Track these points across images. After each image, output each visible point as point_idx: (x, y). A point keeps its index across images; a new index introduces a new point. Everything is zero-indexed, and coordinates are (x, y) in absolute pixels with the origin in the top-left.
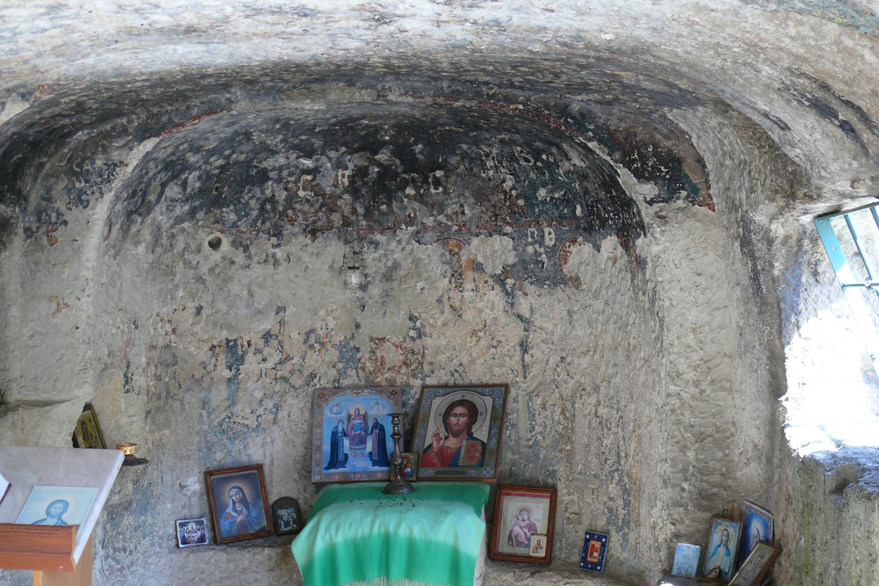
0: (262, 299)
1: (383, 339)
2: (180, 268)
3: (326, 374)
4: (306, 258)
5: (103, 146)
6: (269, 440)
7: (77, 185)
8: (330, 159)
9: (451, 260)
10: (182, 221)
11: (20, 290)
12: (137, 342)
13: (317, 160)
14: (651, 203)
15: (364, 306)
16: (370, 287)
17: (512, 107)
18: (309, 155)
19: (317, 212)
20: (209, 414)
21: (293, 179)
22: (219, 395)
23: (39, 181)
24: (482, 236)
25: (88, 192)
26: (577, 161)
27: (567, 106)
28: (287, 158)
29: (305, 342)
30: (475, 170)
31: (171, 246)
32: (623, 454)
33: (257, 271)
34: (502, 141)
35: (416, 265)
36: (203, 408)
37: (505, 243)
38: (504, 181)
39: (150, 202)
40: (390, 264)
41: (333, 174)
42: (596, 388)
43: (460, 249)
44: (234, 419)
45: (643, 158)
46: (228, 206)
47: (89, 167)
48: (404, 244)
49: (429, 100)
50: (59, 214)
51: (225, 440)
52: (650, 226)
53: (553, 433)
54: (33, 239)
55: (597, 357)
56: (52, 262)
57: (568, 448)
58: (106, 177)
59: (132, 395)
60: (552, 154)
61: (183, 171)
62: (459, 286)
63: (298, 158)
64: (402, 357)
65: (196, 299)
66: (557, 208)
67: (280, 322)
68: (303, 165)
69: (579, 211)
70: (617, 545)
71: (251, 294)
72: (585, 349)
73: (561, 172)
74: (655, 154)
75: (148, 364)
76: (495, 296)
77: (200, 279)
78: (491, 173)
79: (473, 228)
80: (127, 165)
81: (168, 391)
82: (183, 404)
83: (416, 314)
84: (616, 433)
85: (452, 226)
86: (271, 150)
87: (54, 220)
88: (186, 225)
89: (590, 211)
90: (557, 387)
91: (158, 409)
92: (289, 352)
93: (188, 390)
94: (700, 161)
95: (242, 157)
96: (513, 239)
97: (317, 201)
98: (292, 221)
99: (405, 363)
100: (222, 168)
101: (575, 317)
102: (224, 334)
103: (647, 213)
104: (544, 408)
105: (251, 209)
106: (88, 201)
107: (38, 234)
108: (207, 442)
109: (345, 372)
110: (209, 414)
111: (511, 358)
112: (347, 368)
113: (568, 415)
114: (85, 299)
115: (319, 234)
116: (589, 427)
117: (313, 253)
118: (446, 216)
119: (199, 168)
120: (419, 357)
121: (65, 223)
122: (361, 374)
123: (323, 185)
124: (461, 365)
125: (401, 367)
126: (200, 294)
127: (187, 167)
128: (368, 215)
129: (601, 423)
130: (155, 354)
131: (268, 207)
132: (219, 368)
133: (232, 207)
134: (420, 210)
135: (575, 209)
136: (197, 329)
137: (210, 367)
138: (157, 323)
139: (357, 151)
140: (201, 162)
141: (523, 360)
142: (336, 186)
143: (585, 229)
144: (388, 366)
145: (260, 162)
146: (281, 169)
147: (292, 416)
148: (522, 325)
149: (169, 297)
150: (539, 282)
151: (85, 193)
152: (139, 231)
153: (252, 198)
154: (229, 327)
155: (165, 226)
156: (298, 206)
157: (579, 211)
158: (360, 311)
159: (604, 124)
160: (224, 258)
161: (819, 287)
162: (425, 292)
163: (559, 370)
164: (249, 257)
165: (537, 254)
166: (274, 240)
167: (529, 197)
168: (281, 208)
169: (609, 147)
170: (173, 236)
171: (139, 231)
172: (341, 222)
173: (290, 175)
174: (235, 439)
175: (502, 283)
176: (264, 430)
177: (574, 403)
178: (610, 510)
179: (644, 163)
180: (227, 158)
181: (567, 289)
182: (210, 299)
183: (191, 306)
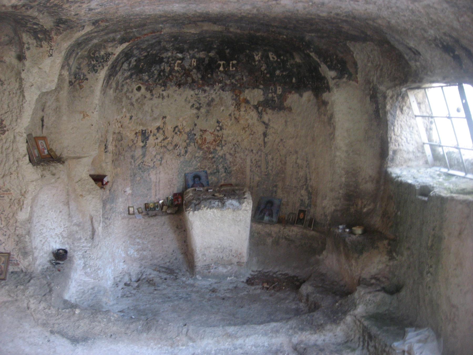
1: (206, 131)
2: (124, 99)
3: (182, 144)
4: (175, 96)
5: (104, 46)
6: (158, 172)
7: (92, 62)
8: (190, 54)
9: (236, 98)
10: (127, 79)
11: (67, 109)
13: (185, 54)
14: (333, 79)
15: (198, 117)
16: (201, 109)
18: (181, 52)
19: (182, 76)
20: (134, 161)
21: (173, 62)
22: (138, 152)
24: (250, 89)
25: (97, 66)
26: (298, 60)
29: (174, 131)
30: (250, 61)
31: (122, 89)
32: (308, 179)
33: (156, 101)
36: (132, 159)
38: (262, 66)
39: (117, 71)
40: (210, 99)
41: (190, 61)
42: (296, 152)
44: (144, 163)
46: (145, 73)
47: (98, 55)
50: (84, 75)
51: (141, 172)
54: (73, 86)
56: (81, 97)
58: (105, 59)
59: (108, 154)
61: (130, 58)
62: (239, 109)
64: (213, 138)
65: (130, 113)
67: (164, 123)
68: (178, 56)
69: (294, 80)
75: (113, 140)
76: (254, 114)
77: (132, 104)
79: (246, 86)
80: (114, 54)
81: (119, 152)
82: (124, 158)
83: (220, 120)
85: (237, 84)
87: (82, 78)
88: (128, 81)
90: (278, 151)
93: (126, 151)
94: (355, 64)
95: (154, 52)
96: (263, 91)
98: (171, 80)
100: (146, 57)
101: (288, 123)
102: (141, 128)
103: (331, 83)
105: (155, 75)
106: (97, 70)
107: (75, 84)
109: (189, 144)
110: (134, 161)
111: (259, 139)
112: (190, 142)
113: (283, 162)
114: (95, 113)
115: (182, 86)
116: (293, 167)
117: (178, 94)
119: (137, 56)
120: (220, 138)
121: (87, 79)
122: (196, 144)
123: (185, 65)
124: (238, 141)
125: (213, 142)
126: (131, 110)
127: (132, 56)
128: (203, 78)
129: (298, 166)
130: (115, 136)
131: (162, 74)
132: (138, 142)
133: (147, 73)
135: (292, 79)
136: (130, 125)
137: (135, 142)
139: (202, 51)
140: (138, 54)
141: (264, 140)
142: (190, 65)
144: (207, 141)
145: (161, 55)
146: (169, 58)
147: (168, 162)
148: (264, 126)
149: (120, 112)
150: (273, 108)
151: (96, 66)
153: (155, 70)
154: (142, 124)
155: (120, 81)
156: (174, 74)
157: (294, 80)
158: (196, 119)
160: (142, 95)
161: (403, 116)
162: (224, 112)
164: (152, 95)
165: (273, 97)
166: (163, 88)
167: (272, 74)
168: (167, 74)
170: (123, 86)
171: (112, 83)
172: (191, 81)
173: (172, 60)
174: (145, 171)
176: (156, 168)
177: (286, 158)
178: (302, 200)
183: (128, 115)
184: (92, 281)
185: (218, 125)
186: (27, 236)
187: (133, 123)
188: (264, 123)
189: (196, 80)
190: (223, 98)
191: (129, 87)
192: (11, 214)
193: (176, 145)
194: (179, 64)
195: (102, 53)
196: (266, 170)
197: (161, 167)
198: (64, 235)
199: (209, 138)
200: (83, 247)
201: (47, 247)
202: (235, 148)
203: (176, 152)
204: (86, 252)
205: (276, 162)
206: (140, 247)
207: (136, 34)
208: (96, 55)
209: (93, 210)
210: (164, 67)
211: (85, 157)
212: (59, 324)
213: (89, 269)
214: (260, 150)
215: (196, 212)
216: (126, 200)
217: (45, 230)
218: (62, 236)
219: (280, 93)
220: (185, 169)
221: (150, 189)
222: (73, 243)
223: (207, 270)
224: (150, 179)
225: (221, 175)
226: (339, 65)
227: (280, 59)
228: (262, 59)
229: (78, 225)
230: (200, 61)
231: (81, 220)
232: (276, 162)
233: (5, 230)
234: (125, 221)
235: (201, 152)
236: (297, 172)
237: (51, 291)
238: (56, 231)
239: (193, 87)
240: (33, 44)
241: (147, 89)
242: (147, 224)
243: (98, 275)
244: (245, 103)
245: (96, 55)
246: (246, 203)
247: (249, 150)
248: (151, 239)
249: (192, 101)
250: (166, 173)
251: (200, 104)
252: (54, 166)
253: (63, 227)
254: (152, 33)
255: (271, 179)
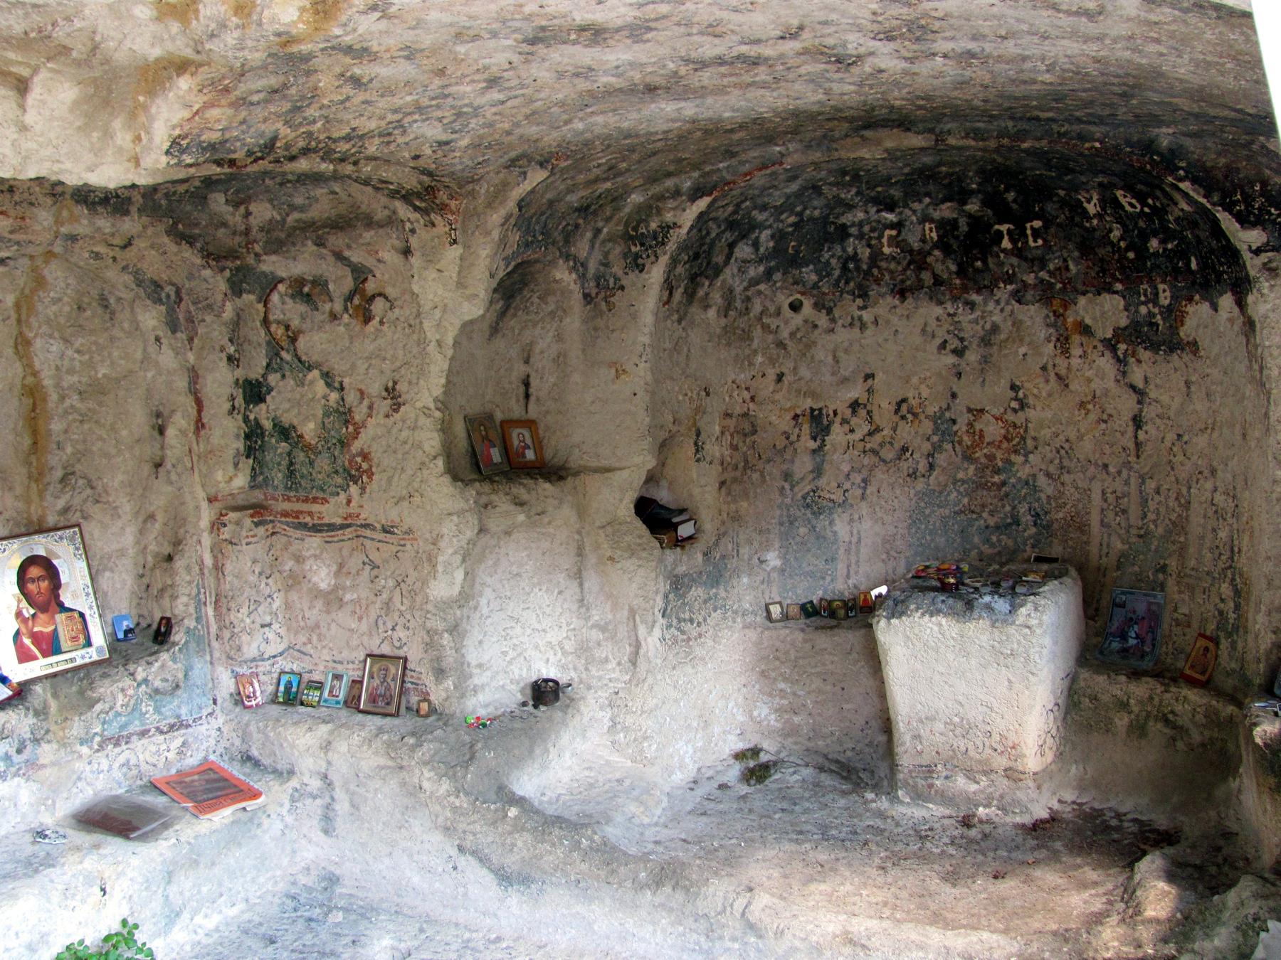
0: (846, 370)
1: (982, 411)
2: (757, 332)
3: (920, 447)
4: (895, 320)
5: (657, 207)
6: (856, 517)
8: (914, 212)
9: (1056, 322)
10: (758, 283)
12: (709, 410)
13: (901, 213)
14: (1257, 252)
17: (1087, 145)
18: (891, 209)
20: (792, 487)
21: (876, 235)
22: (803, 465)
23: (597, 246)
24: (1090, 295)
27: (1152, 141)
28: (867, 212)
29: (897, 412)
30: (1077, 219)
32: (1236, 549)
33: (843, 336)
34: (1101, 185)
35: (1018, 329)
36: (786, 481)
37: (1115, 302)
38: (1111, 230)
40: (988, 326)
41: (919, 228)
42: (1213, 472)
43: (1066, 310)
44: (819, 493)
45: (1248, 199)
48: (1002, 304)
49: (992, 144)
50: (617, 279)
52: (1257, 280)
53: (1167, 521)
55: (1215, 435)
57: (1182, 539)
60: (1158, 198)
62: (1066, 352)
63: (878, 211)
64: (1003, 431)
66: (1171, 262)
69: (1194, 265)
70: (1226, 653)
71: (836, 360)
72: (1203, 426)
73: (1171, 218)
74: (1263, 193)
75: (723, 433)
76: (1105, 363)
77: (781, 345)
78: (1095, 222)
81: (746, 462)
82: (762, 476)
83: (1018, 383)
84: (1231, 525)
86: (847, 204)
87: (611, 285)
88: (762, 287)
89: (1204, 265)
90: (1173, 469)
91: (735, 480)
92: (878, 423)
93: (769, 461)
95: (817, 213)
96: (1124, 297)
97: (905, 258)
98: (878, 281)
99: (1005, 437)
101: (1193, 388)
102: (808, 403)
103: (1253, 265)
104: (1158, 493)
106: (644, 265)
108: (789, 516)
110: (792, 487)
113: (1183, 501)
114: (642, 365)
115: (907, 294)
116: (1205, 516)
118: (1049, 272)
119: (770, 226)
121: (622, 288)
122: (958, 448)
123: (910, 241)
128: (961, 272)
129: (1216, 512)
130: (731, 423)
131: (851, 266)
132: (803, 439)
133: (811, 267)
134: (1019, 266)
136: (777, 397)
137: (794, 438)
138: (733, 390)
139: (943, 202)
140: (771, 220)
141: (1136, 437)
142: (923, 241)
143: (1201, 285)
144: (987, 440)
145: (837, 218)
148: (1134, 397)
150: (1154, 347)
152: (707, 294)
153: (831, 256)
154: (813, 395)
156: (883, 264)
157: (1194, 265)
159: (1198, 160)
160: (806, 321)
162: (1029, 359)
163: (1175, 449)
164: (833, 320)
165: (1151, 315)
166: (859, 302)
167: (1142, 252)
168: (865, 267)
169: (1204, 188)
170: (748, 299)
171: (707, 294)
173: (873, 230)
175: (1113, 349)
176: (852, 506)
177: (1190, 488)
178: (1221, 613)
179: (1249, 205)
180: (800, 214)
181: (1184, 355)
182: (792, 365)
183: (772, 373)
184: (629, 763)
185: (1013, 394)
186: (446, 635)
187: (784, 390)
188: (1133, 387)
189: (945, 276)
190: (1021, 321)
191: (768, 303)
192: (418, 584)
193: (904, 449)
194: (890, 237)
195: (653, 225)
196: (1140, 523)
197: (864, 505)
198: (567, 647)
199: (993, 430)
200: (610, 680)
201: (521, 669)
202: (1061, 458)
203: (904, 465)
204: (617, 693)
205: (1167, 498)
206: (785, 702)
207: (724, 173)
208: (641, 231)
209: (637, 596)
210: (855, 249)
211: (620, 469)
212: (474, 835)
213: (622, 735)
214: (1127, 464)
215: (895, 621)
216: (763, 582)
217: (518, 630)
218: (562, 649)
219: (1167, 302)
220: (927, 512)
221: (833, 559)
222: (587, 669)
223: (926, 778)
224: (835, 533)
225: (1025, 531)
226: (1273, 210)
227: (1149, 206)
228: (1103, 209)
229: (603, 629)
230: (947, 227)
231: (610, 617)
232: (1167, 498)
233: (408, 617)
234: (752, 635)
235: (972, 468)
236: (1214, 530)
237: (472, 758)
238: (549, 635)
239: (940, 296)
240: (418, 221)
241: (818, 306)
242: (808, 646)
243: (642, 751)
244: (1080, 333)
245: (641, 231)
246: (1029, 605)
247: (1096, 465)
248: (814, 686)
249: (941, 334)
250: (876, 521)
251: (962, 340)
252: (525, 486)
253: (565, 628)
254: (760, 170)
255: (1153, 547)
